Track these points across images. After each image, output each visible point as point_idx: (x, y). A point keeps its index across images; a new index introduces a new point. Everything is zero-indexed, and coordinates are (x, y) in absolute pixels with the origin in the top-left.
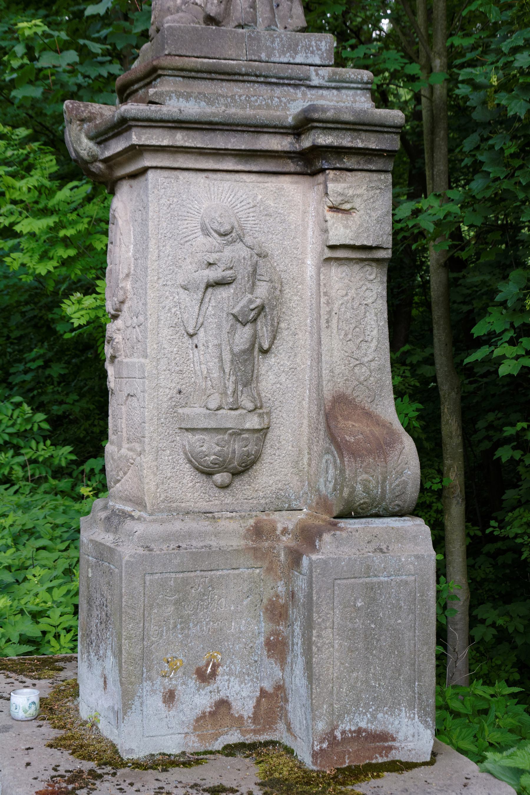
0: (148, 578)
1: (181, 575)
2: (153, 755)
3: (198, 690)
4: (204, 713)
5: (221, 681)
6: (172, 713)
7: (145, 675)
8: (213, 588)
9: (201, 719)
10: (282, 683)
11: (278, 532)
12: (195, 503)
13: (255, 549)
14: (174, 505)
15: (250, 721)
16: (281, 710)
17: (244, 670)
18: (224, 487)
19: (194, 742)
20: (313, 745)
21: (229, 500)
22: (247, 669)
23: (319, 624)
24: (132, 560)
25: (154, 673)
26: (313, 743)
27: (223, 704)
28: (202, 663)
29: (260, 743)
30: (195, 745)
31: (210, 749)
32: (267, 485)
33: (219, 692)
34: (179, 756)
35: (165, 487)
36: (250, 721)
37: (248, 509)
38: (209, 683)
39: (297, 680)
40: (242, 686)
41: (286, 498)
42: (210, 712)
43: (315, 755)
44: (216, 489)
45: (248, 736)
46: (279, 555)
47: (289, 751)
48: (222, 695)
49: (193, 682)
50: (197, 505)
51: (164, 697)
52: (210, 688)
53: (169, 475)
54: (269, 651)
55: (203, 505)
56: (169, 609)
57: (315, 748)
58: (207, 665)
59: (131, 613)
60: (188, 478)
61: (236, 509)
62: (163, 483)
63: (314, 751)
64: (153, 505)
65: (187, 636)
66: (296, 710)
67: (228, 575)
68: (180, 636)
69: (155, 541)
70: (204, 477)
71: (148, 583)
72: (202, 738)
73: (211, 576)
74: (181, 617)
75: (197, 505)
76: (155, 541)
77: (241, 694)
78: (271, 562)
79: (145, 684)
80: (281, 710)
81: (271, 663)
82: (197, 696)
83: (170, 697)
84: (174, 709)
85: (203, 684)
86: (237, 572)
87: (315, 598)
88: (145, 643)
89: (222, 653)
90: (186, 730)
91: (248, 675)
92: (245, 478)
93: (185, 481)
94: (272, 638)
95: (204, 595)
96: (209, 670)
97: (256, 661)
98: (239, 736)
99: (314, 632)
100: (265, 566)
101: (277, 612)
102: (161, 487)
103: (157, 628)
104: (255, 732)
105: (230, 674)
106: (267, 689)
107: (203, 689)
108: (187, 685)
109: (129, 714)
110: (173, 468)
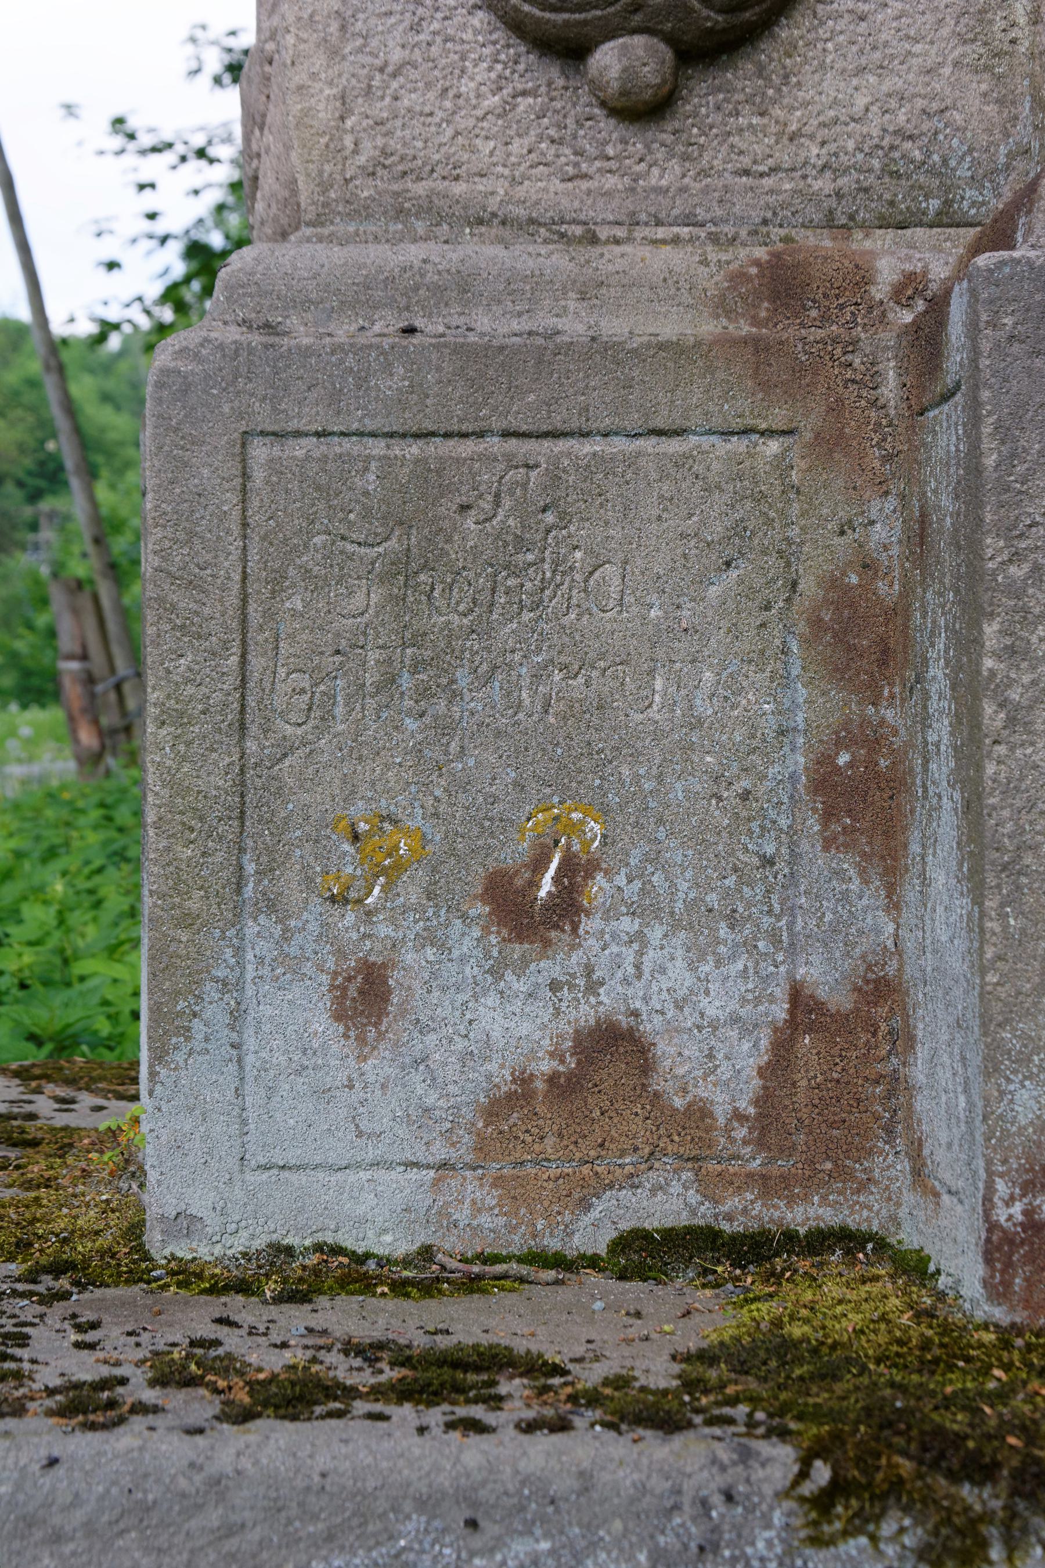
0: (260, 451)
1: (414, 449)
2: (289, 1251)
3: (495, 972)
4: (524, 1080)
5: (602, 938)
6: (377, 1067)
7: (249, 890)
8: (565, 519)
9: (512, 1104)
10: (891, 970)
11: (880, 292)
12: (513, 181)
13: (757, 345)
14: (420, 189)
15: (741, 1132)
16: (890, 1094)
17: (712, 899)
18: (643, 110)
19: (477, 1209)
20: (988, 1200)
21: (667, 174)
22: (727, 894)
23: (1016, 591)
24: (186, 367)
25: (290, 883)
26: (990, 1187)
27: (613, 1049)
28: (514, 852)
29: (790, 1236)
30: (485, 1220)
31: (553, 1244)
32: (843, 114)
33: (593, 987)
34: (406, 1262)
35: (380, 109)
36: (741, 1132)
37: (756, 216)
38: (547, 943)
39: (937, 926)
40: (705, 969)
41: (932, 172)
42: (552, 1079)
43: (998, 1248)
44: (607, 126)
45: (732, 1203)
46: (873, 379)
47: (915, 1268)
48: (609, 1001)
49: (470, 939)
50: (520, 192)
51: (339, 992)
52: (550, 968)
53: (397, 56)
54: (828, 816)
55: (547, 192)
56: (358, 601)
57: (1001, 1215)
58: (539, 864)
59: (184, 602)
60: (481, 73)
61: (701, 214)
62: (369, 90)
63: (992, 1227)
64: (325, 187)
65: (445, 728)
66: (939, 1078)
67: (631, 461)
68: (411, 724)
69: (305, 304)
70: (554, 71)
71: (258, 475)
72: (513, 1192)
73: (555, 461)
74: (418, 639)
75: (520, 192)
76: (305, 304)
77: (707, 1016)
78: (837, 408)
79: (251, 929)
80: (890, 1094)
81: (839, 874)
82: (492, 999)
83: (366, 997)
84: (384, 1050)
85: (518, 950)
86: (673, 446)
87: (990, 461)
88: (251, 745)
89: (604, 812)
90: (440, 1152)
91: (733, 921)
92: (741, 76)
93: (466, 86)
94: (843, 759)
95: (521, 544)
96: (546, 886)
97: (768, 862)
98: (693, 1197)
99: (990, 629)
100: (809, 426)
101: (862, 640)
102: (360, 105)
103: (304, 681)
104: (767, 1185)
105: (646, 909)
106: (822, 993)
107: (522, 967)
108: (443, 947)
109: (179, 1057)
110: (416, 28)
